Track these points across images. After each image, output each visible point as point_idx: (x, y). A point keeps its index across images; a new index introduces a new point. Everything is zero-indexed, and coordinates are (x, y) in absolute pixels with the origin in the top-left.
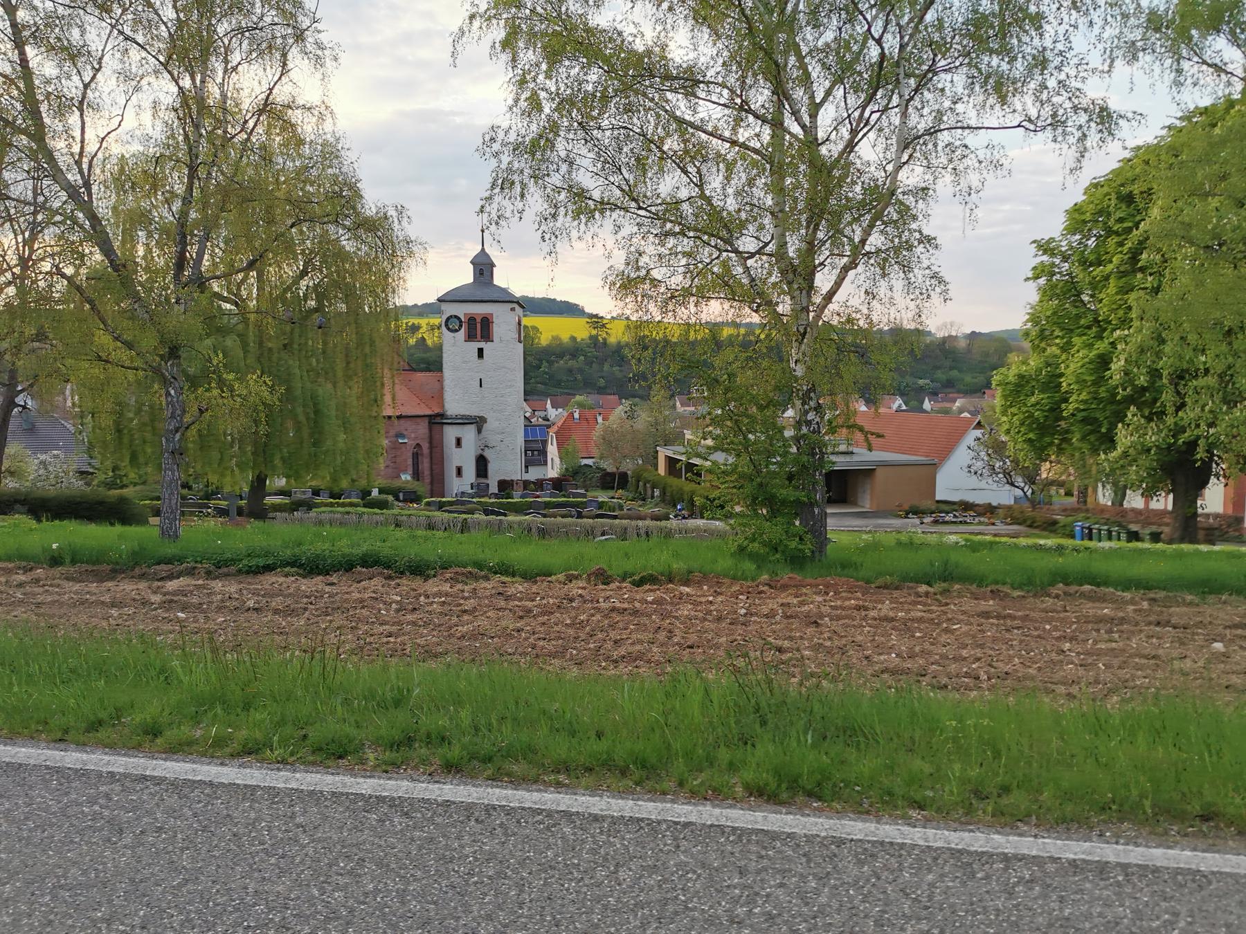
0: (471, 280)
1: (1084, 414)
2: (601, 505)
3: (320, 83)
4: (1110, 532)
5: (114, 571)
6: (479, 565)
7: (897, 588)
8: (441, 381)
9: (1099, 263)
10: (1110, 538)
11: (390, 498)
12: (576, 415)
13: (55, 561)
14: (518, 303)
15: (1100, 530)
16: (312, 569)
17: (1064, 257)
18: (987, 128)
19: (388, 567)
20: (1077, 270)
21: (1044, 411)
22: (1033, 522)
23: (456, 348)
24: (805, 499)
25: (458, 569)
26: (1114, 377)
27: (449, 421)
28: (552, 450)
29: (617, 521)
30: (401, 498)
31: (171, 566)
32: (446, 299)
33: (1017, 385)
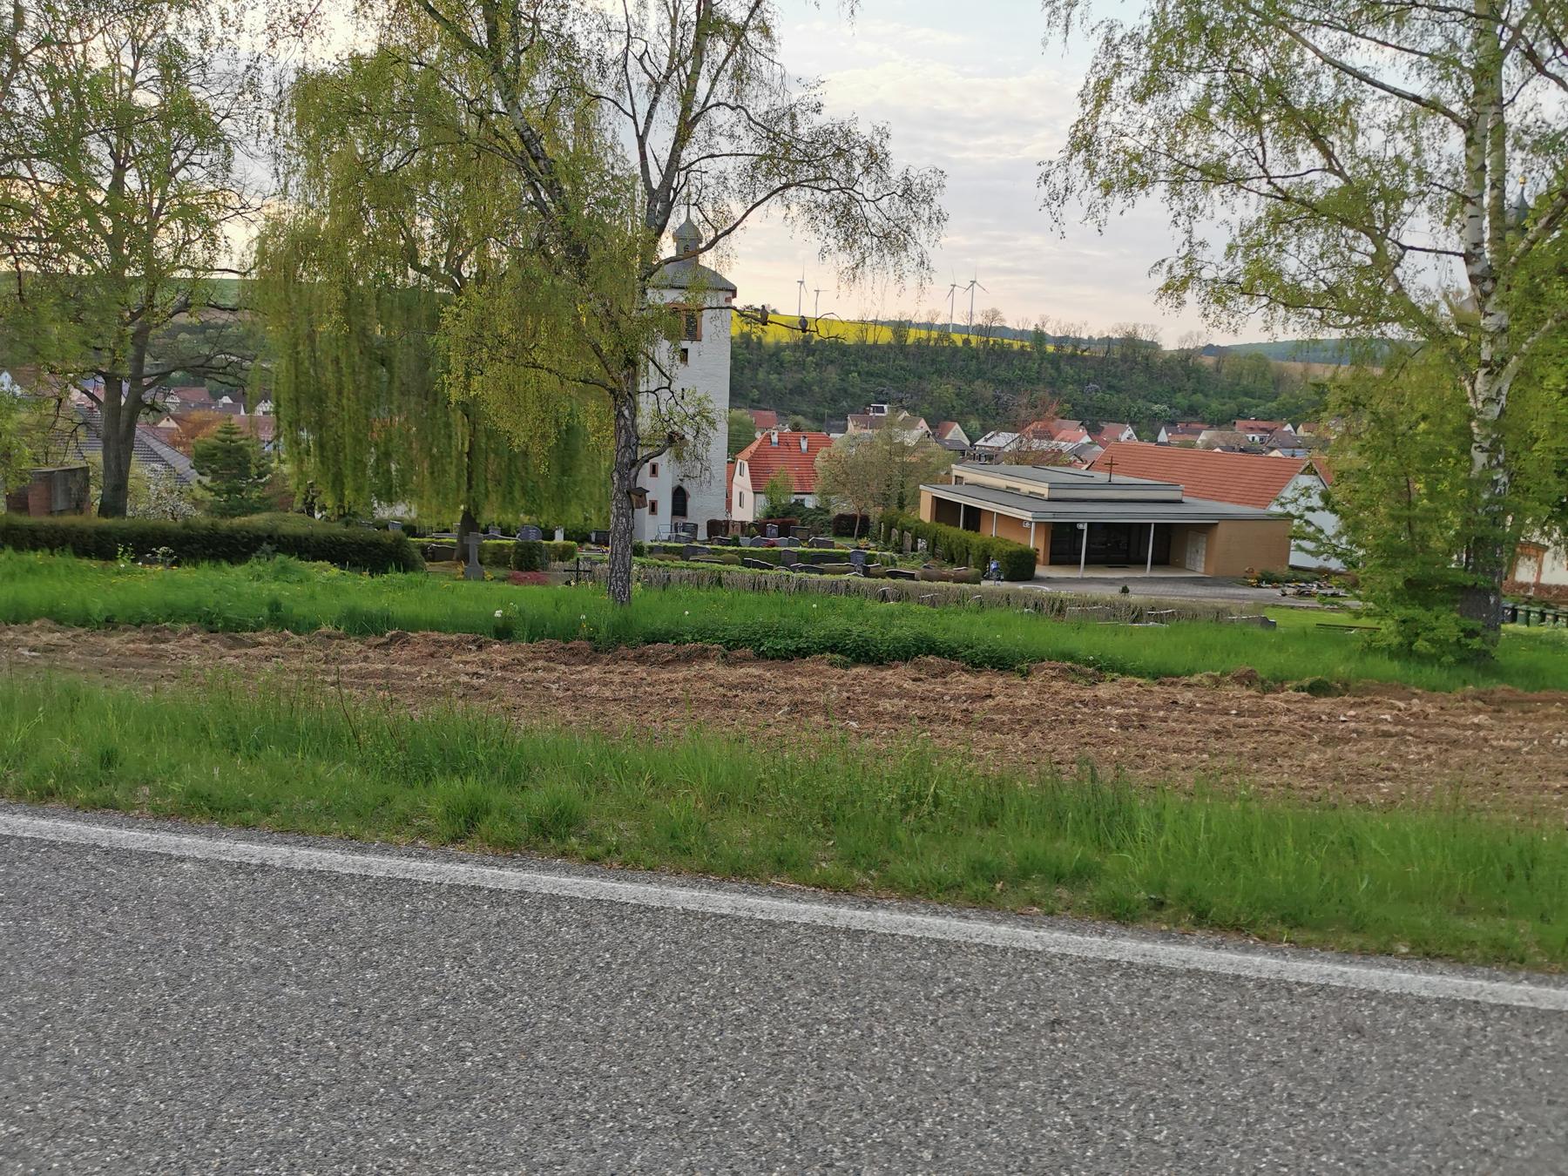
4: (1515, 611)
12: (775, 439)
13: (504, 632)
15: (1528, 612)
16: (859, 656)
29: (826, 577)
30: (593, 539)
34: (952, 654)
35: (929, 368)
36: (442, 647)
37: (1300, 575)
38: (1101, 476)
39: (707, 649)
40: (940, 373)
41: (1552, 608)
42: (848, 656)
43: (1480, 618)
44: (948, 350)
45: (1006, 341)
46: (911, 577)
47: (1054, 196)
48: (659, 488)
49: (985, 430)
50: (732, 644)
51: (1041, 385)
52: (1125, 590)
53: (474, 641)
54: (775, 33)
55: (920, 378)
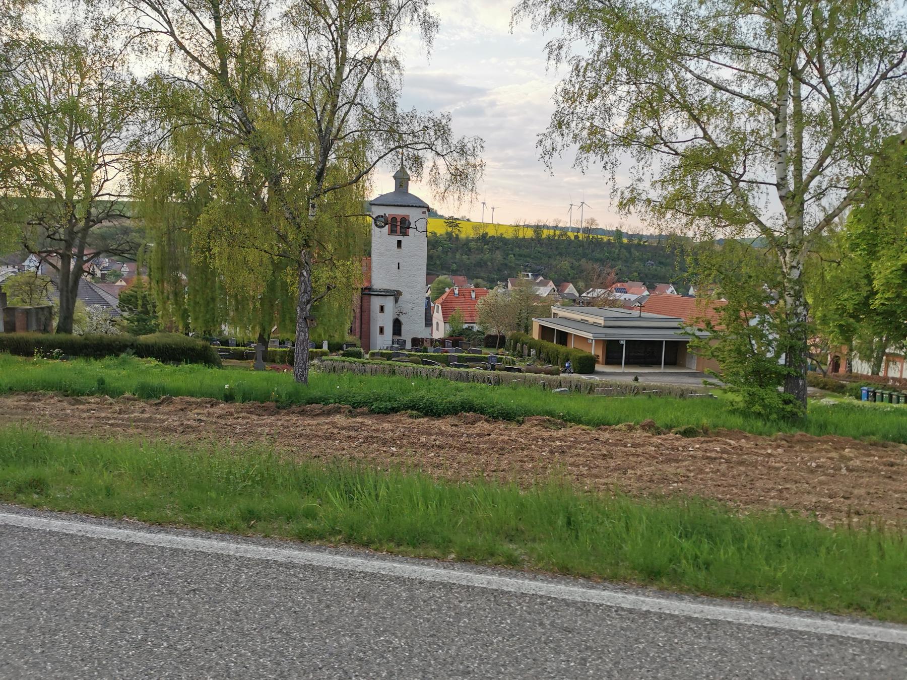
0: (393, 189)
4: (891, 396)
6: (551, 413)
10: (891, 401)
12: (456, 292)
13: (229, 398)
15: (882, 394)
16: (427, 411)
22: (826, 385)
23: (381, 238)
28: (438, 317)
32: (376, 203)
34: (482, 411)
36: (190, 405)
38: (636, 313)
39: (340, 408)
40: (561, 254)
41: (897, 391)
42: (421, 412)
43: (792, 393)
45: (599, 236)
46: (519, 370)
47: (546, 153)
48: (385, 320)
49: (587, 287)
50: (356, 405)
51: (620, 262)
52: (636, 379)
53: (210, 402)
54: (402, 64)
55: (549, 257)
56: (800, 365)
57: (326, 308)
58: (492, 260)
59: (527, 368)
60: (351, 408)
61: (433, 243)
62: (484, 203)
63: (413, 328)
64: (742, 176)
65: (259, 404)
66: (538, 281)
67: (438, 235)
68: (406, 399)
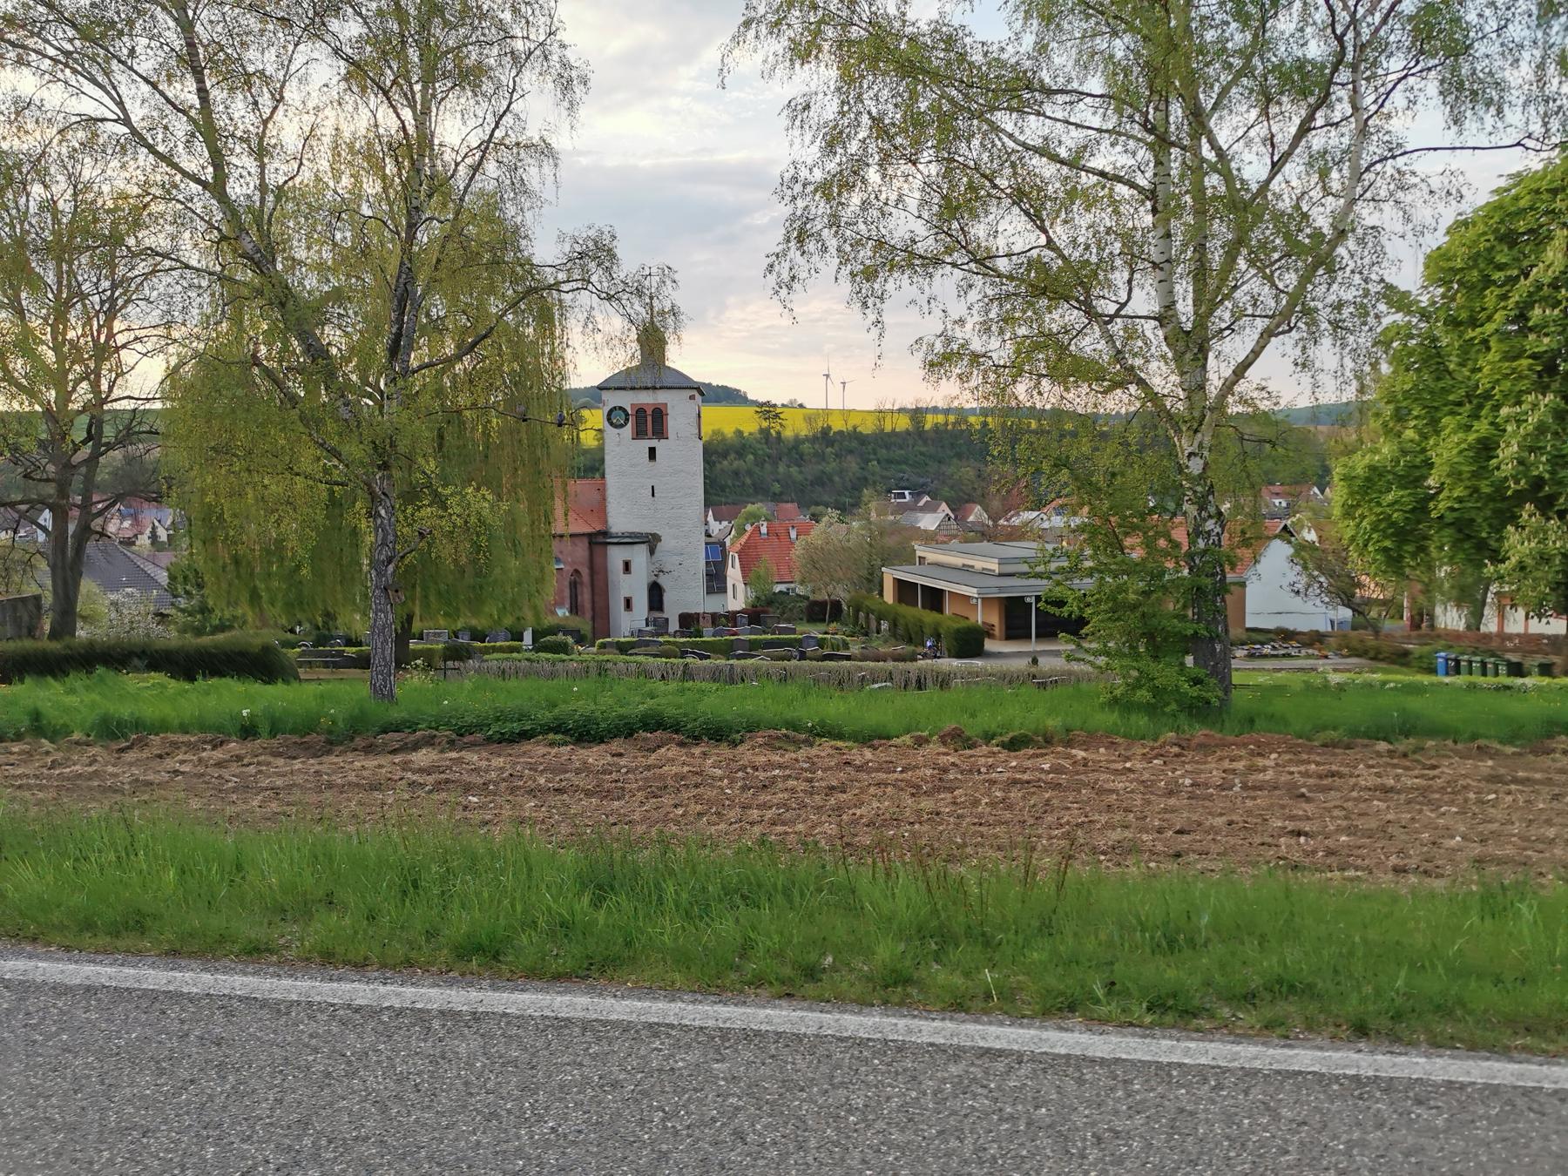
1: (1455, 515)
2: (821, 643)
3: (566, 113)
4: (1484, 664)
5: (330, 743)
6: (794, 726)
7: (1348, 747)
8: (602, 490)
9: (1474, 323)
11: (570, 640)
12: (764, 530)
13: (248, 731)
14: (698, 389)
15: (1470, 662)
16: (581, 735)
17: (1423, 316)
18: (1474, 148)
19: (677, 732)
20: (1439, 329)
21: (1406, 512)
23: (623, 449)
24: (1205, 633)
25: (771, 732)
26: (1503, 467)
27: (615, 540)
28: (734, 574)
31: (402, 735)
33: (1368, 479)
34: (676, 728)
35: (949, 452)
37: (1255, 636)
40: (959, 456)
44: (966, 434)
48: (633, 586)
52: (1035, 661)
56: (1214, 618)
57: (498, 571)
58: (841, 472)
59: (862, 654)
60: (454, 736)
61: (715, 453)
62: (827, 376)
63: (687, 595)
64: (1123, 305)
65: (296, 738)
66: (921, 504)
67: (746, 434)
68: (546, 716)
